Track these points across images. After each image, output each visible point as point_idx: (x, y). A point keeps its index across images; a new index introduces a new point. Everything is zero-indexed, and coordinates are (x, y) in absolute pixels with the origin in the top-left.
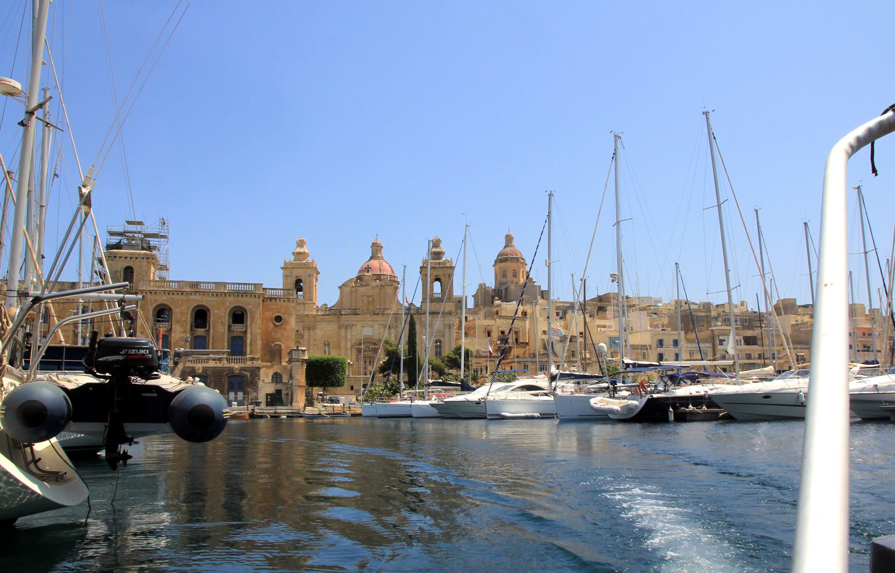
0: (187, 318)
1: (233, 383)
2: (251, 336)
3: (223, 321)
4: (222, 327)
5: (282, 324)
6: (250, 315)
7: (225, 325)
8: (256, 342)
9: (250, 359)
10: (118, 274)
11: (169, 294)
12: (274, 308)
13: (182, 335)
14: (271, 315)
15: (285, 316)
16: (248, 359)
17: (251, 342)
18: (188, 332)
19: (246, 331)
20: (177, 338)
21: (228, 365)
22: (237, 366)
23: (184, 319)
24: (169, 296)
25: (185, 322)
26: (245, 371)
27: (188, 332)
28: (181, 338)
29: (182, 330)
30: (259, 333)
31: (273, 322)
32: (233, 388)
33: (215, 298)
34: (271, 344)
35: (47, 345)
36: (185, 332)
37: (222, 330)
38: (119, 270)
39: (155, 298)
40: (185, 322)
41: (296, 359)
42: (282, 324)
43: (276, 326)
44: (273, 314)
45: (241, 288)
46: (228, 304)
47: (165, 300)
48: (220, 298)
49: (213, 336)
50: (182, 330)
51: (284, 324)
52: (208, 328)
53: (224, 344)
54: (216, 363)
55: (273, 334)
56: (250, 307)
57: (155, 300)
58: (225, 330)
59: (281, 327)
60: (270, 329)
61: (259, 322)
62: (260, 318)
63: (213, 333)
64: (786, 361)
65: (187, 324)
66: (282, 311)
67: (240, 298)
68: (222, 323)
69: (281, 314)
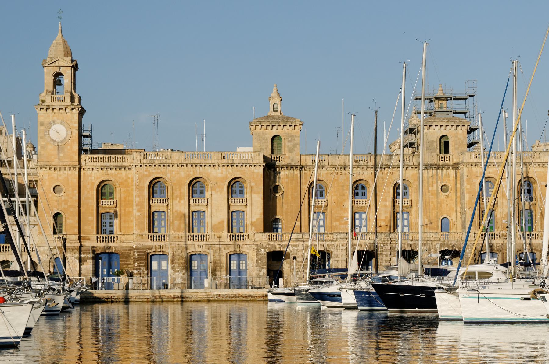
10: (435, 144)
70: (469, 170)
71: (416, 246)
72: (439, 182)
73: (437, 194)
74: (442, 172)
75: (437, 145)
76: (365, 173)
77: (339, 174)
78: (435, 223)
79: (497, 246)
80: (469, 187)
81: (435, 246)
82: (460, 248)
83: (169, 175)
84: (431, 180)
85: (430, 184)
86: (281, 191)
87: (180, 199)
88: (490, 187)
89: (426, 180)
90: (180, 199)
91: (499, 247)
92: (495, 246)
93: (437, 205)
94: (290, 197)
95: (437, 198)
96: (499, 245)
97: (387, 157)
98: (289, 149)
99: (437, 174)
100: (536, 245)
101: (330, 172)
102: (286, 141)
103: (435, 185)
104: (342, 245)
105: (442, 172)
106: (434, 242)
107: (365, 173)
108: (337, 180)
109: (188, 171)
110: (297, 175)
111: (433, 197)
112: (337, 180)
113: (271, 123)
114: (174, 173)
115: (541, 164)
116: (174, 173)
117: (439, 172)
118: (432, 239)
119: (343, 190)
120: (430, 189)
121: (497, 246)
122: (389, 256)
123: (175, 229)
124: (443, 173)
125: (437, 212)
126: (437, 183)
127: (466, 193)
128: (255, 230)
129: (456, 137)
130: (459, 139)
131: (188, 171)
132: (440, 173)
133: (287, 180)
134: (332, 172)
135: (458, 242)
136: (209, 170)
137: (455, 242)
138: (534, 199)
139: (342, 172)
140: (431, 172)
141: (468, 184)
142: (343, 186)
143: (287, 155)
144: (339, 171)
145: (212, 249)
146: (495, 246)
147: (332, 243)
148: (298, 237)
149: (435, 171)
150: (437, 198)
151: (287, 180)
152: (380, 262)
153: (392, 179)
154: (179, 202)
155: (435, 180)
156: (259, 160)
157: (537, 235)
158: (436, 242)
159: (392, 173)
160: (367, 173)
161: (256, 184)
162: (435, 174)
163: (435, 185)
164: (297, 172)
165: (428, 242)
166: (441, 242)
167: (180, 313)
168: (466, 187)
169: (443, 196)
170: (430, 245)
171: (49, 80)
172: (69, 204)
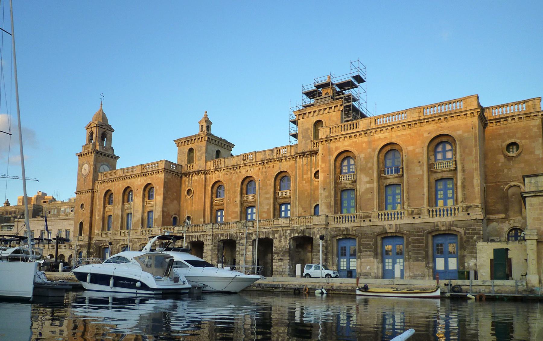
0: (373, 164)
1: (441, 246)
2: (463, 175)
3: (420, 159)
4: (419, 168)
5: (519, 155)
6: (460, 144)
7: (423, 164)
8: (472, 182)
9: (463, 209)
10: (309, 131)
11: (350, 136)
12: (504, 134)
13: (368, 186)
14: (500, 145)
15: (523, 141)
16: (460, 209)
17: (463, 183)
18: (375, 181)
19: (456, 169)
20: (363, 189)
21: (431, 220)
22: (443, 219)
23: (369, 165)
24: (351, 141)
25: (371, 168)
26: (456, 226)
27: (375, 181)
28: (367, 189)
29: (368, 179)
30: (476, 169)
31: (503, 154)
32: (442, 253)
33: (408, 131)
34: (502, 187)
35: (155, 198)
36: (371, 181)
37: (419, 172)
38: (309, 127)
39: (337, 145)
40: (371, 168)
41: (533, 192)
42: (519, 155)
43: (509, 159)
44: (503, 142)
45: (445, 109)
46: (426, 135)
47: (347, 146)
48: (415, 130)
49: (408, 181)
50: (368, 179)
51: (522, 154)
52: (401, 173)
53: (423, 191)
54: (414, 218)
55: (506, 171)
56: (459, 132)
57: (337, 148)
58: (423, 171)
59: (519, 158)
60: (500, 165)
61: (474, 151)
62: (476, 146)
63: (408, 178)
64: (39, 337)
65: (373, 172)
66: (518, 135)
67: (443, 124)
68: (419, 162)
69: (518, 138)
70: (324, 147)
71: (269, 234)
72: (313, 169)
73: (311, 180)
74: (316, 158)
75: (311, 132)
76: (252, 170)
77: (233, 173)
78: (309, 211)
79: (352, 230)
80: (323, 165)
81: (286, 232)
82: (310, 234)
83: (114, 188)
84: (305, 168)
85: (305, 171)
86: (191, 194)
87: (118, 205)
88: (351, 163)
89: (301, 168)
90: (118, 205)
91: (355, 230)
92: (351, 230)
93: (311, 193)
94: (197, 197)
95: (311, 185)
96: (355, 228)
97: (270, 151)
98: (198, 158)
99: (311, 161)
100: (401, 226)
101: (226, 172)
102: (197, 152)
103: (309, 172)
104: (209, 236)
105: (316, 158)
106: (284, 229)
107: (252, 170)
108: (230, 179)
109: (123, 183)
110: (202, 178)
111: (307, 184)
112: (230, 179)
113: (180, 141)
114: (116, 185)
115: (406, 124)
116: (116, 185)
117: (313, 158)
118: (282, 225)
119: (235, 187)
120: (305, 176)
121: (352, 230)
122: (245, 244)
123: (114, 228)
124: (317, 159)
125: (311, 200)
126: (311, 170)
127: (321, 173)
128: (157, 225)
129: (330, 119)
130: (333, 121)
131: (123, 183)
132: (314, 159)
133: (196, 184)
134: (227, 172)
135: (308, 227)
136: (134, 180)
137: (305, 227)
138: (401, 170)
139: (235, 171)
140: (305, 160)
141: (323, 162)
142: (235, 184)
143: (197, 163)
144: (232, 171)
145: (132, 242)
146: (351, 230)
147: (203, 234)
148: (180, 230)
149: (309, 159)
150: (311, 185)
151: (196, 184)
152: (238, 251)
153: (273, 172)
154: (118, 207)
155: (309, 168)
156: (162, 167)
157: (403, 213)
158: (286, 229)
159: (273, 167)
160: (254, 170)
161: (159, 187)
162: (310, 160)
163: (309, 172)
164: (203, 176)
165: (279, 229)
166: (291, 228)
167: (526, 310)
168: (321, 166)
169: (316, 183)
170: (281, 232)
171: (321, 175)
172: (86, 215)
